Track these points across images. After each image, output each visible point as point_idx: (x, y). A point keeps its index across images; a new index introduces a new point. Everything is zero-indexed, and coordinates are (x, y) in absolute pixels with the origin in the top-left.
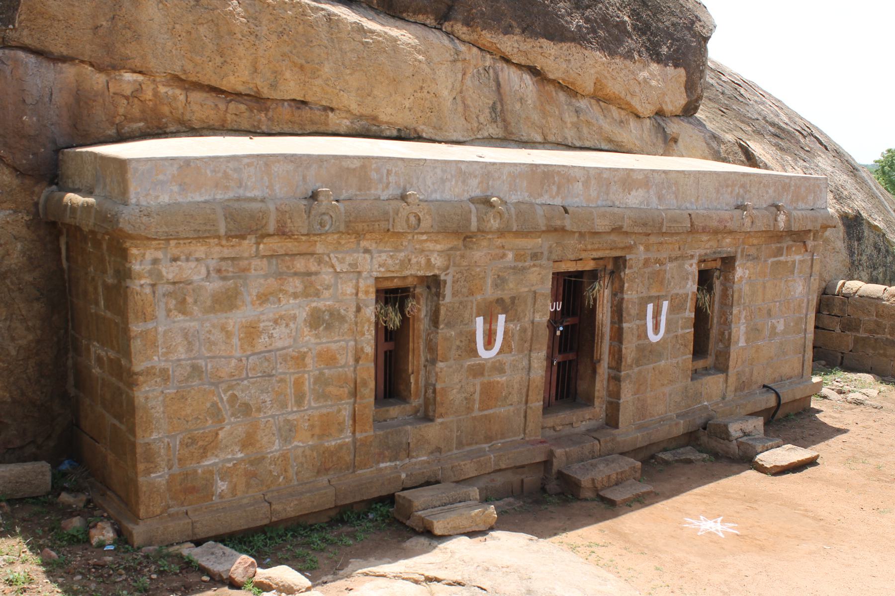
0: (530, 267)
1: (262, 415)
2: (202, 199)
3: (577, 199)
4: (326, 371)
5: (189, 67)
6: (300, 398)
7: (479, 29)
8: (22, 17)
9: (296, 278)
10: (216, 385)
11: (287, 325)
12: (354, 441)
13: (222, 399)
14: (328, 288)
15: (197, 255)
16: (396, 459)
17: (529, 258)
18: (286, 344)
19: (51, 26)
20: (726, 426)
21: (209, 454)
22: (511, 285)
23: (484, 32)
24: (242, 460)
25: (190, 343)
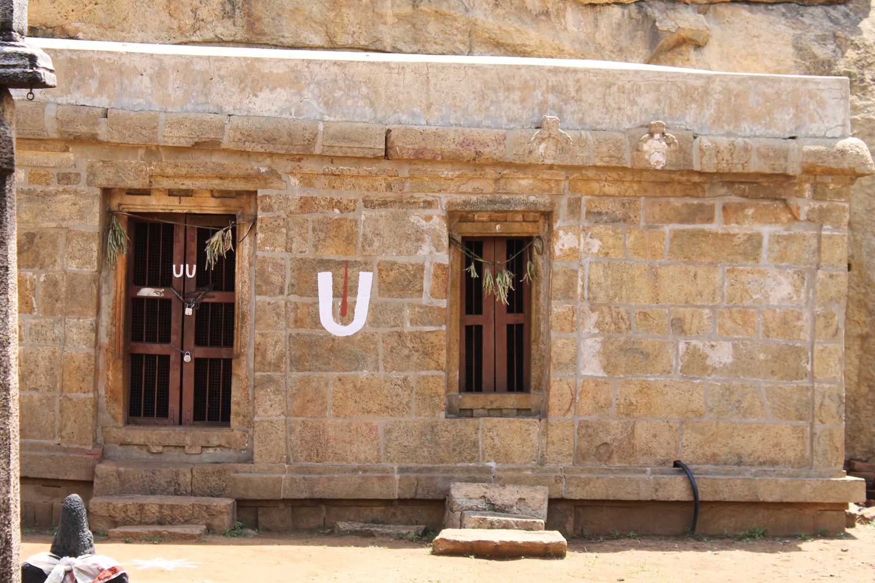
0: (57, 193)
3: (141, 101)
20: (447, 492)
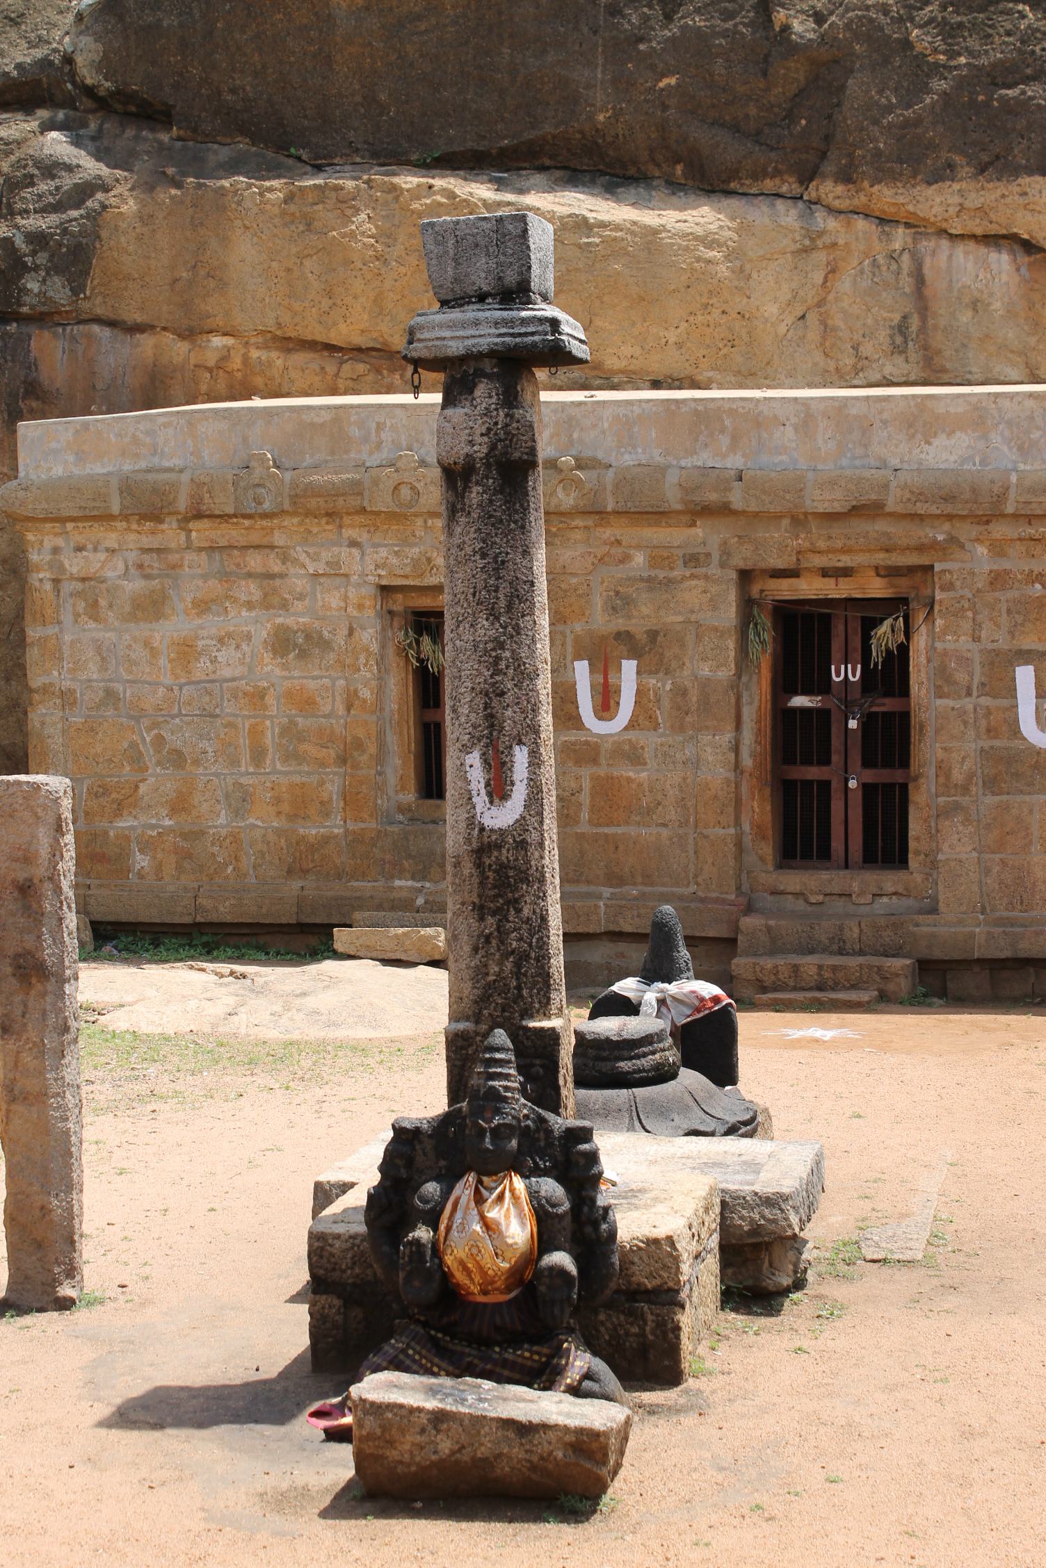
0: (684, 578)
1: (201, 770)
2: (105, 471)
3: (784, 457)
4: (300, 720)
5: (286, 318)
6: (258, 755)
7: (866, 184)
8: (95, 282)
9: (250, 581)
10: (137, 719)
11: (238, 647)
12: (347, 831)
13: (144, 739)
14: (301, 597)
15: (108, 544)
16: (424, 878)
17: (680, 562)
18: (237, 673)
19: (126, 289)
21: (125, 813)
22: (645, 610)
23: (876, 187)
24: (171, 830)
25: (103, 659)
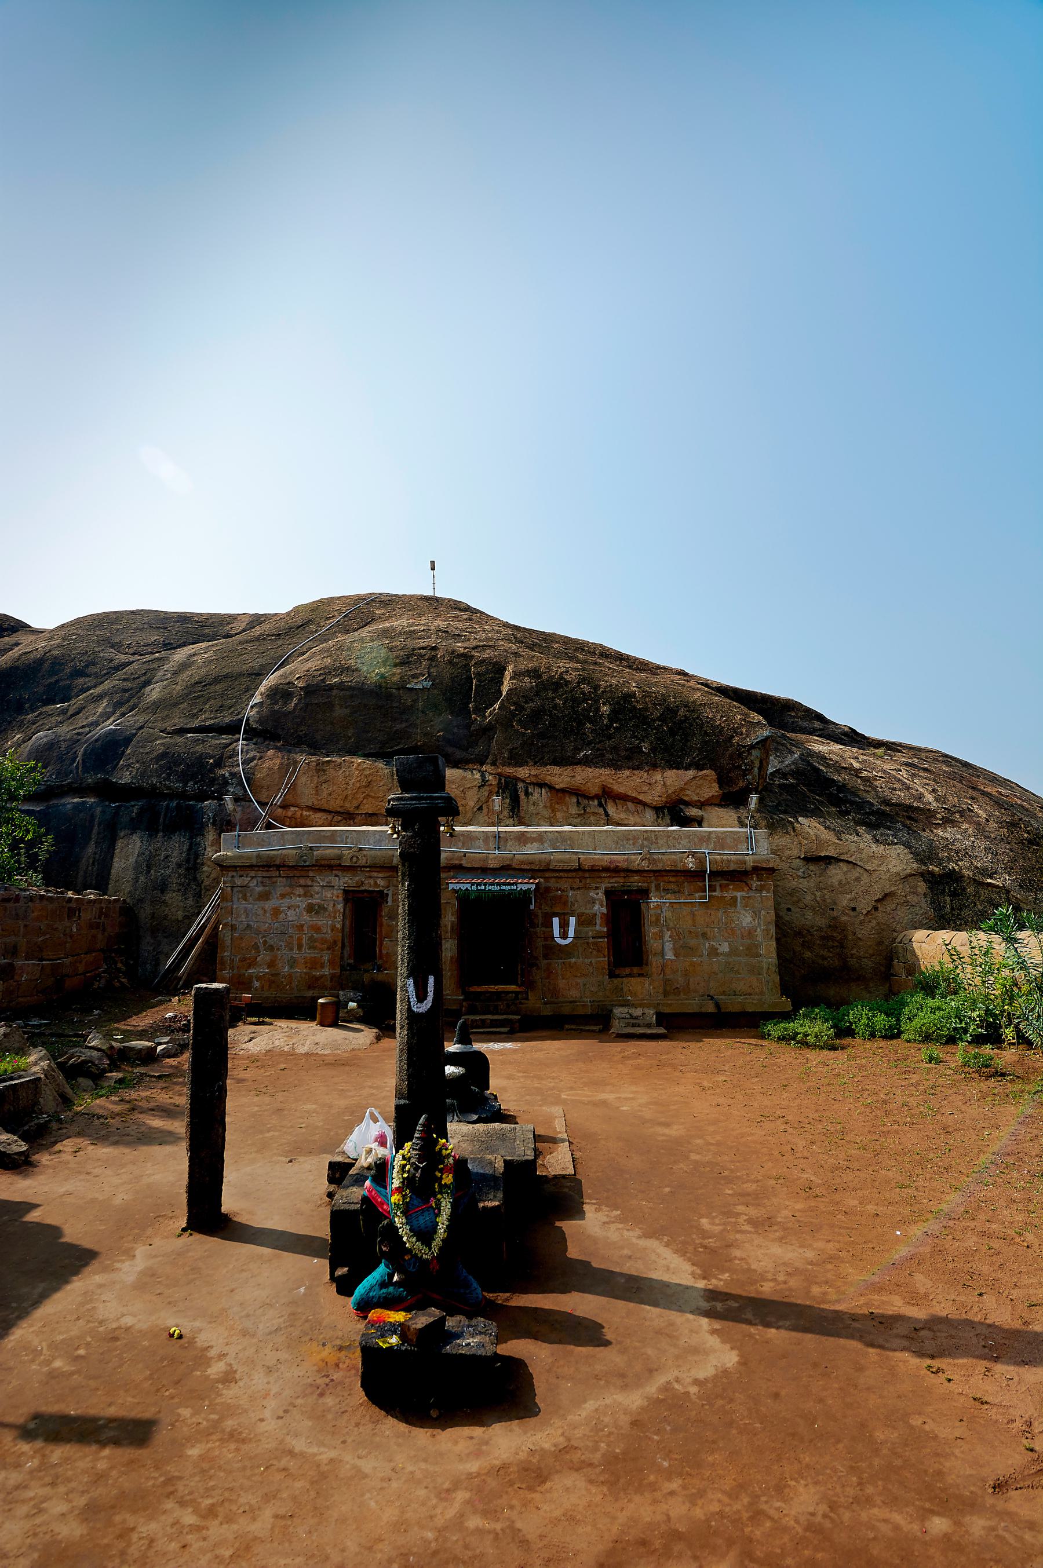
6: (300, 947)
